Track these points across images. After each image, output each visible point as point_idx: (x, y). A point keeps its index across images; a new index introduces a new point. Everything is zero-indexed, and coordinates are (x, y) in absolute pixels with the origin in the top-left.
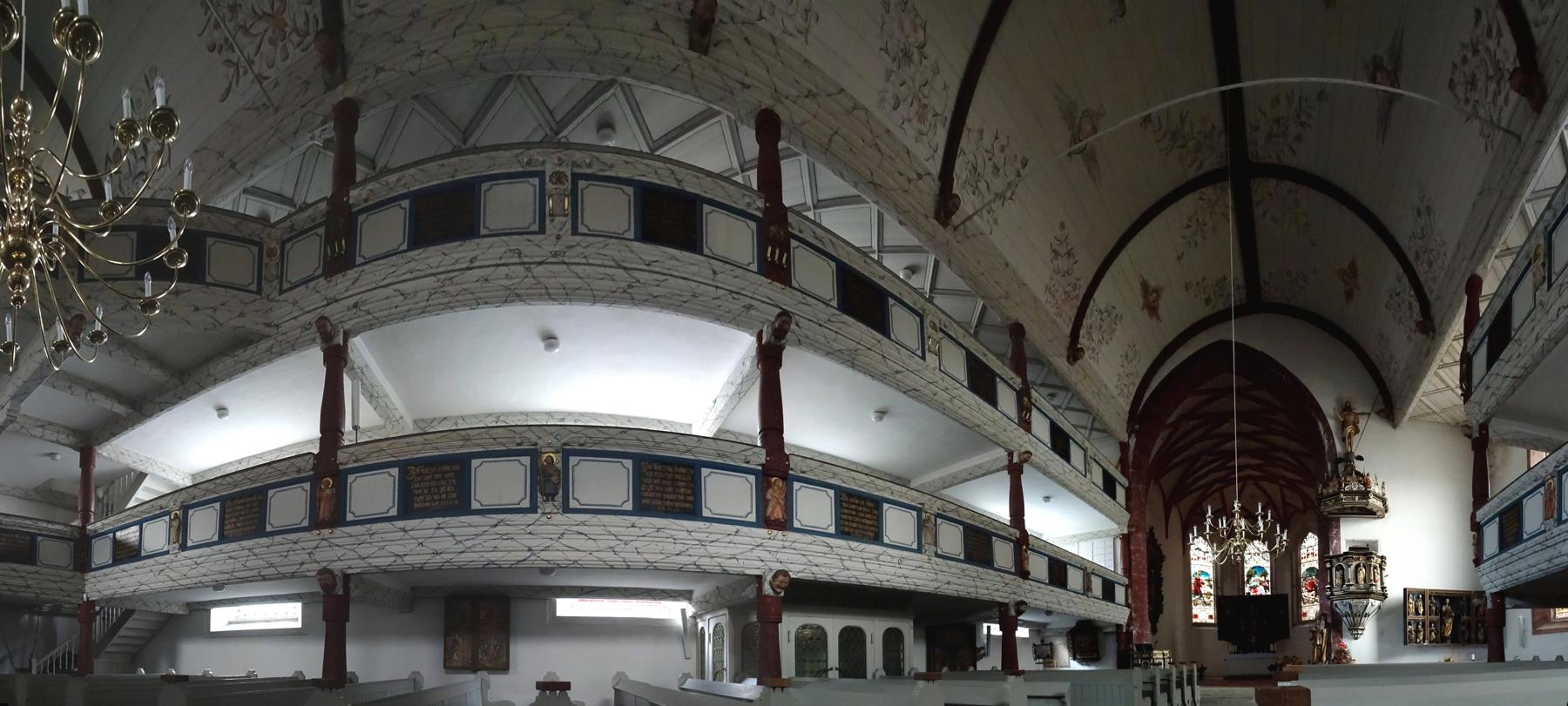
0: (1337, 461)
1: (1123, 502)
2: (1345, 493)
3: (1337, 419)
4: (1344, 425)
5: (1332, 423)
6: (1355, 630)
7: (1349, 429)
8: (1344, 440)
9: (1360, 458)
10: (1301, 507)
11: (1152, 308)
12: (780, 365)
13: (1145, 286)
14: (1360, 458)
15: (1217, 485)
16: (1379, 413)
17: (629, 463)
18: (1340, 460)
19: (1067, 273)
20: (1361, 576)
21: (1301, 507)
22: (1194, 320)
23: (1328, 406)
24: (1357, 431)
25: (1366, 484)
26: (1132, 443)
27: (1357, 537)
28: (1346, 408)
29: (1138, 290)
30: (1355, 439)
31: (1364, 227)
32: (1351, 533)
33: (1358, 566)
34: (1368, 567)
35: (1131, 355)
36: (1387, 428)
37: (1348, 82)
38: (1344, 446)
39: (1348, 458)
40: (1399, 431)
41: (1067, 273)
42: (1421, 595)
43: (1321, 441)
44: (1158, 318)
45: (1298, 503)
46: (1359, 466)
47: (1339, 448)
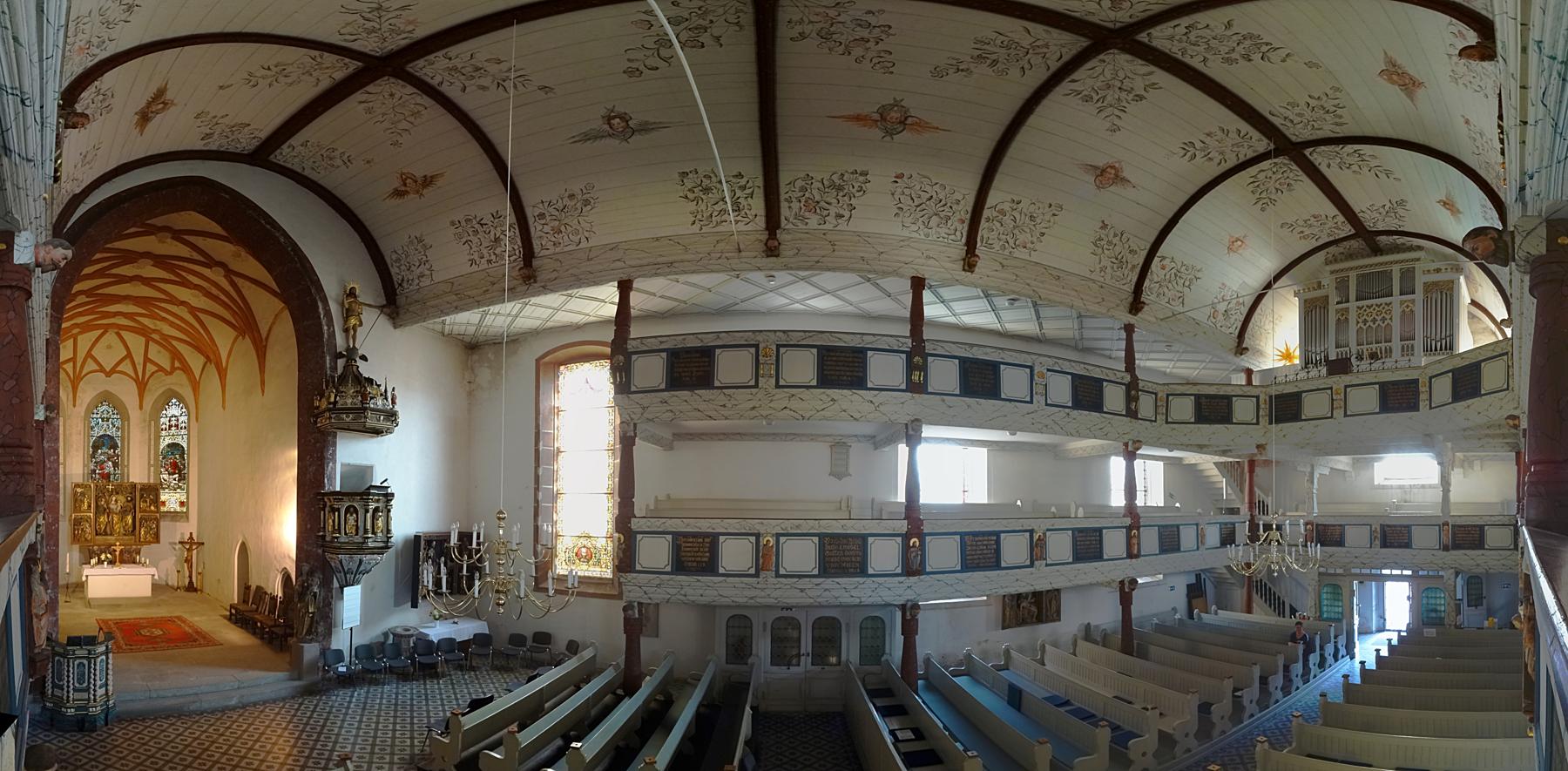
7: (353, 321)
8: (346, 331)
9: (364, 358)
10: (167, 367)
11: (144, 117)
13: (160, 93)
14: (364, 358)
15: (76, 331)
16: (381, 308)
17: (815, 351)
18: (340, 355)
19: (108, 24)
20: (380, 523)
21: (167, 367)
22: (981, 171)
23: (331, 288)
27: (352, 461)
29: (153, 89)
31: (1032, 120)
32: (350, 452)
35: (89, 158)
39: (351, 354)
40: (399, 333)
41: (108, 24)
43: (320, 324)
44: (921, 126)
46: (365, 370)
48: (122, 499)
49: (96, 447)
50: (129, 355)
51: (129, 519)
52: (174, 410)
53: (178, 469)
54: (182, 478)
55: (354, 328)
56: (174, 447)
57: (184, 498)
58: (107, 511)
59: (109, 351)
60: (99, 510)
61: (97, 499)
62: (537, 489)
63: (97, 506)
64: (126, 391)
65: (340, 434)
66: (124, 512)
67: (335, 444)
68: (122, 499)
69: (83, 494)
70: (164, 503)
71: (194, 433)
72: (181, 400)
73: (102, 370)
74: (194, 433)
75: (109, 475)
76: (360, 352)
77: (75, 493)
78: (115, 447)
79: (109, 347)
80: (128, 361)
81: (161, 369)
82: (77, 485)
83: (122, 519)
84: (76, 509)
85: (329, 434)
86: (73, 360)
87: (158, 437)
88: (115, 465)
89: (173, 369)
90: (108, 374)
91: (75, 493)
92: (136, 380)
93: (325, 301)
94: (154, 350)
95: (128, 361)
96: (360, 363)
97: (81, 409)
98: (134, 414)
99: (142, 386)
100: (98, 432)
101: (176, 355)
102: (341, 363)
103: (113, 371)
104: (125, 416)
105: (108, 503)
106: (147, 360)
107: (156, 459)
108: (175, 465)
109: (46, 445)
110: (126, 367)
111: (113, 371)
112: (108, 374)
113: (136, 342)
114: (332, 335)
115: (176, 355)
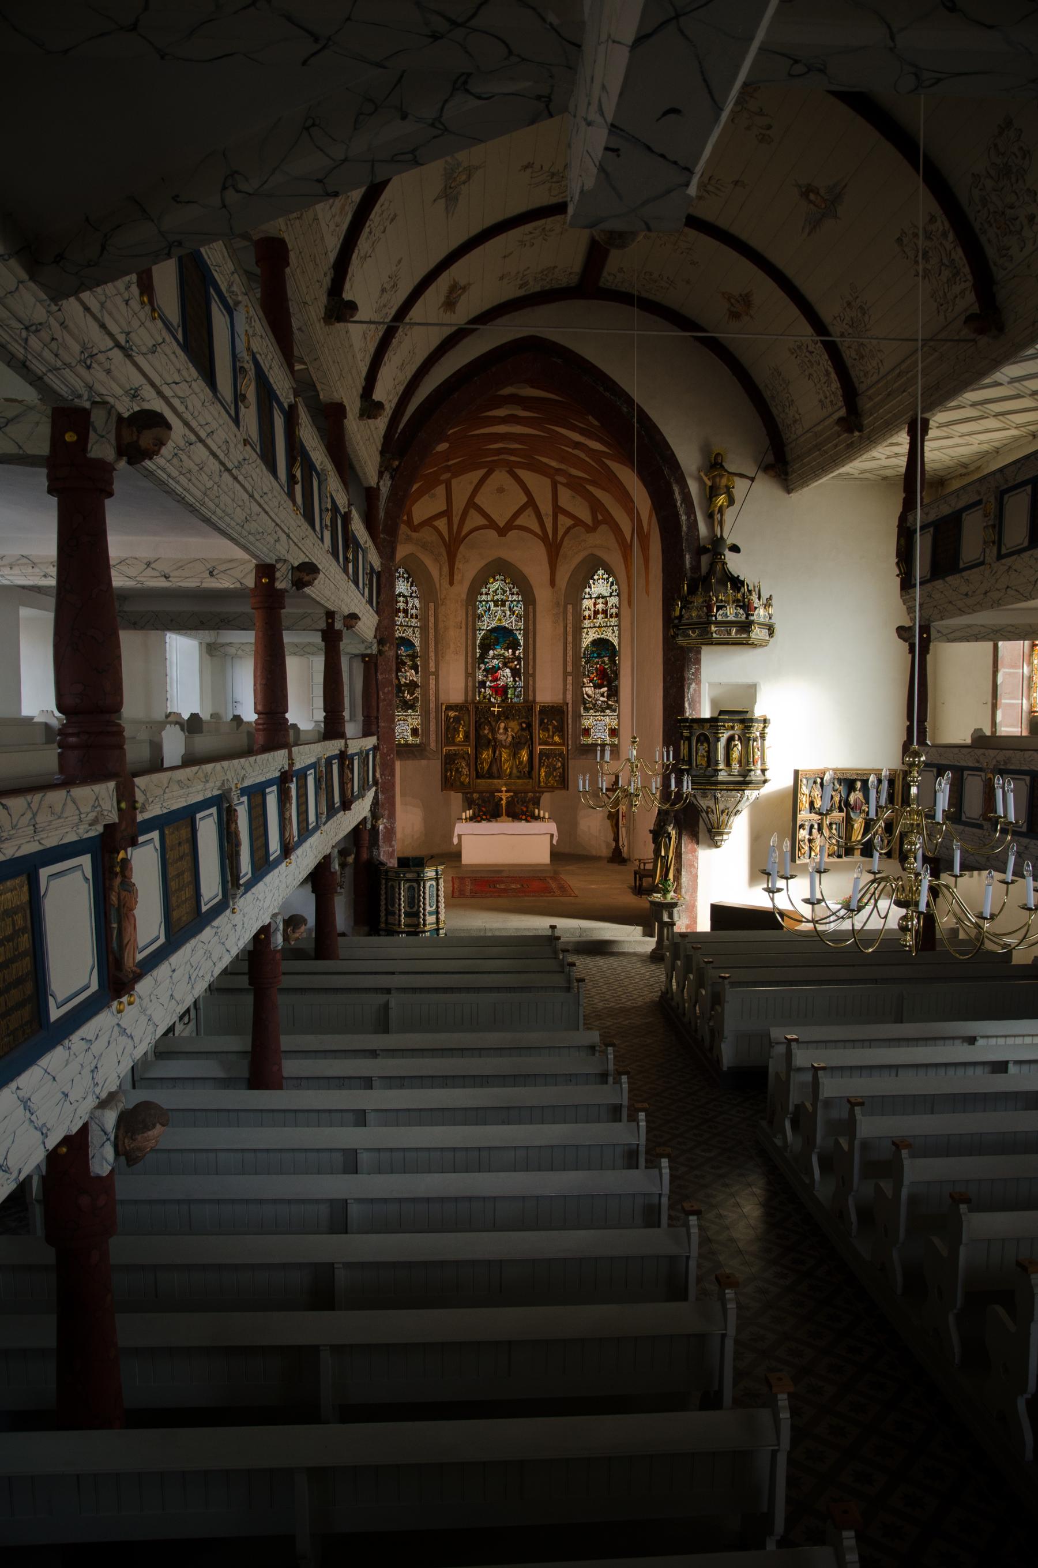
0: (701, 551)
1: (173, 312)
2: (718, 623)
3: (700, 481)
4: (712, 493)
5: (693, 487)
6: (713, 835)
7: (722, 500)
8: (710, 516)
9: (735, 549)
12: (489, 821)
16: (766, 468)
20: (735, 754)
23: (689, 458)
24: (731, 501)
25: (747, 608)
26: (385, 489)
27: (724, 680)
28: (714, 465)
30: (729, 515)
33: (731, 739)
34: (746, 740)
36: (779, 493)
37: (760, 35)
38: (711, 526)
39: (716, 546)
42: (819, 780)
43: (677, 516)
45: (584, 513)
46: (734, 564)
47: (703, 529)
48: (514, 725)
49: (485, 647)
50: (531, 502)
51: (524, 755)
52: (600, 586)
53: (608, 679)
54: (614, 693)
55: (721, 511)
56: (602, 645)
57: (614, 724)
58: (494, 744)
59: (501, 496)
60: (481, 743)
61: (478, 727)
62: (994, 707)
63: (478, 737)
64: (533, 561)
65: (704, 648)
66: (515, 747)
67: (698, 661)
68: (514, 725)
69: (457, 720)
70: (587, 732)
71: (626, 623)
72: (609, 571)
73: (492, 524)
74: (626, 623)
75: (505, 688)
76: (729, 542)
77: (447, 718)
78: (514, 645)
79: (501, 490)
80: (529, 511)
81: (578, 522)
82: (450, 707)
83: (515, 754)
84: (449, 740)
85: (690, 650)
86: (447, 513)
87: (578, 630)
88: (515, 673)
89: (597, 524)
90: (502, 532)
91: (447, 718)
92: (544, 538)
93: (684, 486)
94: (566, 498)
95: (529, 511)
96: (730, 557)
97: (461, 589)
98: (543, 595)
99: (554, 551)
100: (487, 624)
101: (596, 506)
102: (705, 560)
103: (510, 526)
104: (529, 600)
105: (493, 731)
106: (558, 510)
107: (576, 658)
108: (602, 674)
109: (380, 677)
110: (528, 520)
111: (510, 526)
112: (502, 532)
113: (539, 485)
114: (693, 525)
115: (596, 506)
